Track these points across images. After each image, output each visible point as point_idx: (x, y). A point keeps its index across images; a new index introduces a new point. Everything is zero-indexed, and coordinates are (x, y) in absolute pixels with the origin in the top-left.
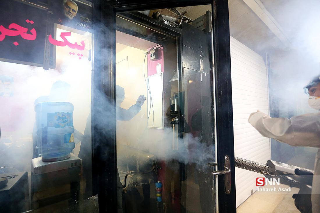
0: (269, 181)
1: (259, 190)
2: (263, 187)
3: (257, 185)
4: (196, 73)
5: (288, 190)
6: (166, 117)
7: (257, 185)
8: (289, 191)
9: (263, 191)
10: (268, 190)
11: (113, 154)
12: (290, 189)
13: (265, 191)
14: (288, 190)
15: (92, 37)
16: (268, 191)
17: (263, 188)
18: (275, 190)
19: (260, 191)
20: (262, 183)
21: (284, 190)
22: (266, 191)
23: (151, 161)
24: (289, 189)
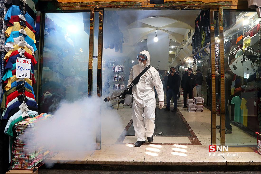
0: (225, 148)
1: (211, 155)
2: (215, 153)
3: (209, 151)
4: (122, 99)
5: (235, 155)
6: (74, 102)
7: (209, 151)
8: (236, 156)
9: (215, 156)
10: (213, 155)
11: (32, 30)
12: (237, 154)
13: (216, 156)
14: (235, 155)
15: (42, 65)
16: (213, 156)
17: (215, 153)
18: (215, 155)
19: (217, 156)
20: (214, 149)
21: (232, 155)
22: (217, 156)
23: (59, 109)
24: (236, 154)
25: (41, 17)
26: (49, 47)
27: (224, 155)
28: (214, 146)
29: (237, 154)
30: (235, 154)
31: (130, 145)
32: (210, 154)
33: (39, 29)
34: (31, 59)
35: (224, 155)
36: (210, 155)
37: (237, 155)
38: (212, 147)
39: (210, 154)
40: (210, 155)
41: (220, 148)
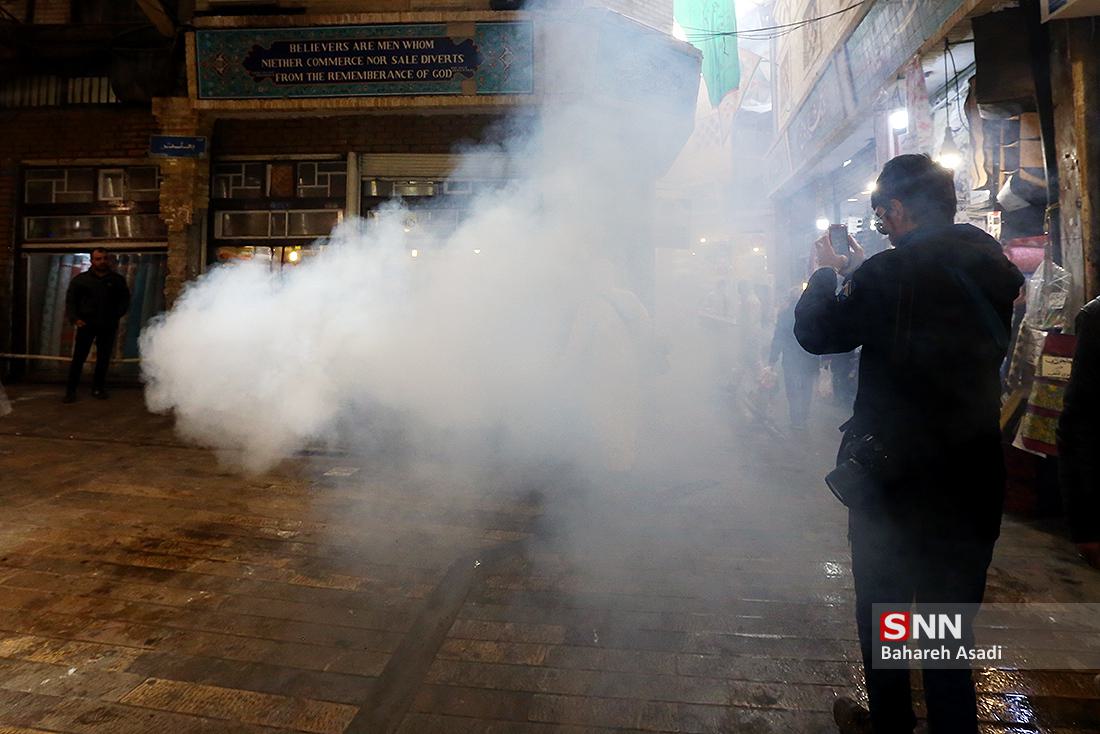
9: (86, 100)
12: (997, 649)
14: (991, 654)
21: (976, 653)
25: (281, 157)
26: (149, 365)
27: (946, 654)
28: (902, 617)
29: (1000, 651)
30: (989, 651)
31: (431, 99)
32: (886, 650)
33: (444, 97)
34: (70, 101)
35: (946, 654)
36: (883, 652)
37: (997, 656)
38: (894, 621)
39: (886, 650)
40: (886, 655)
41: (946, 628)
